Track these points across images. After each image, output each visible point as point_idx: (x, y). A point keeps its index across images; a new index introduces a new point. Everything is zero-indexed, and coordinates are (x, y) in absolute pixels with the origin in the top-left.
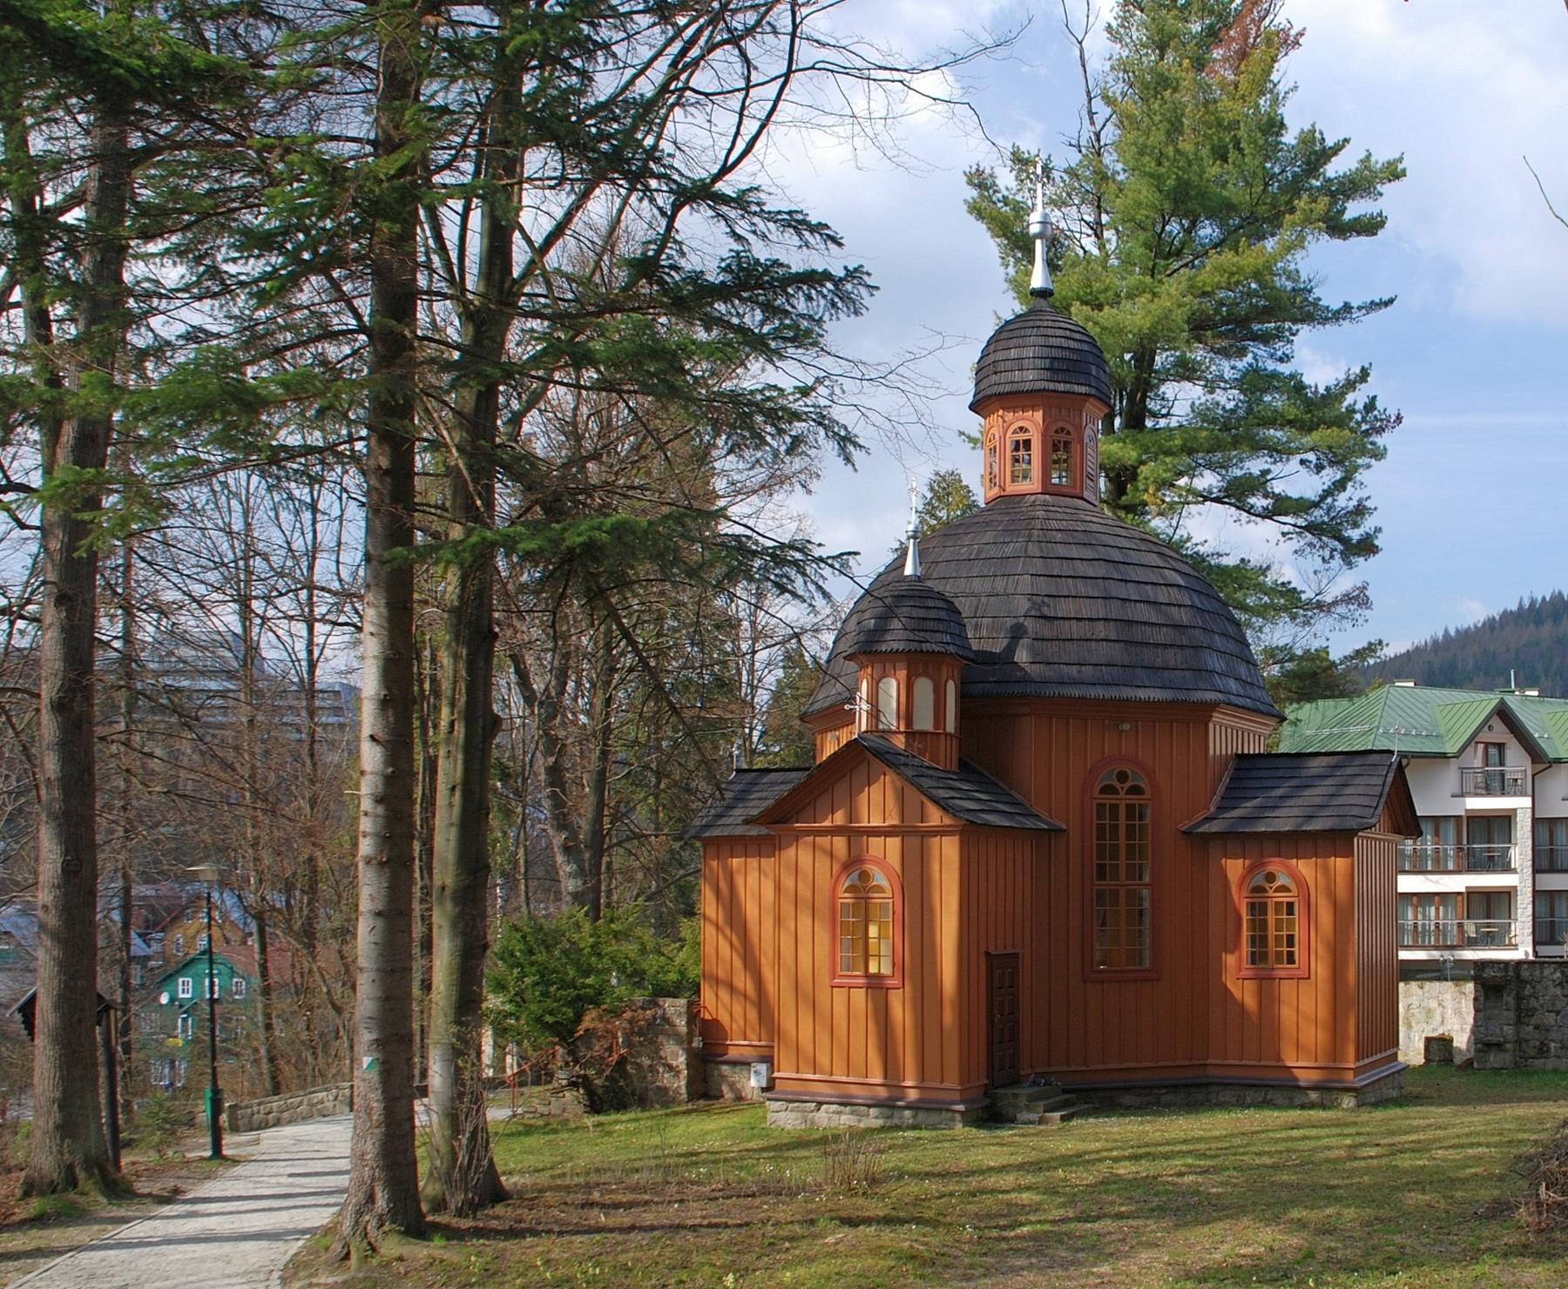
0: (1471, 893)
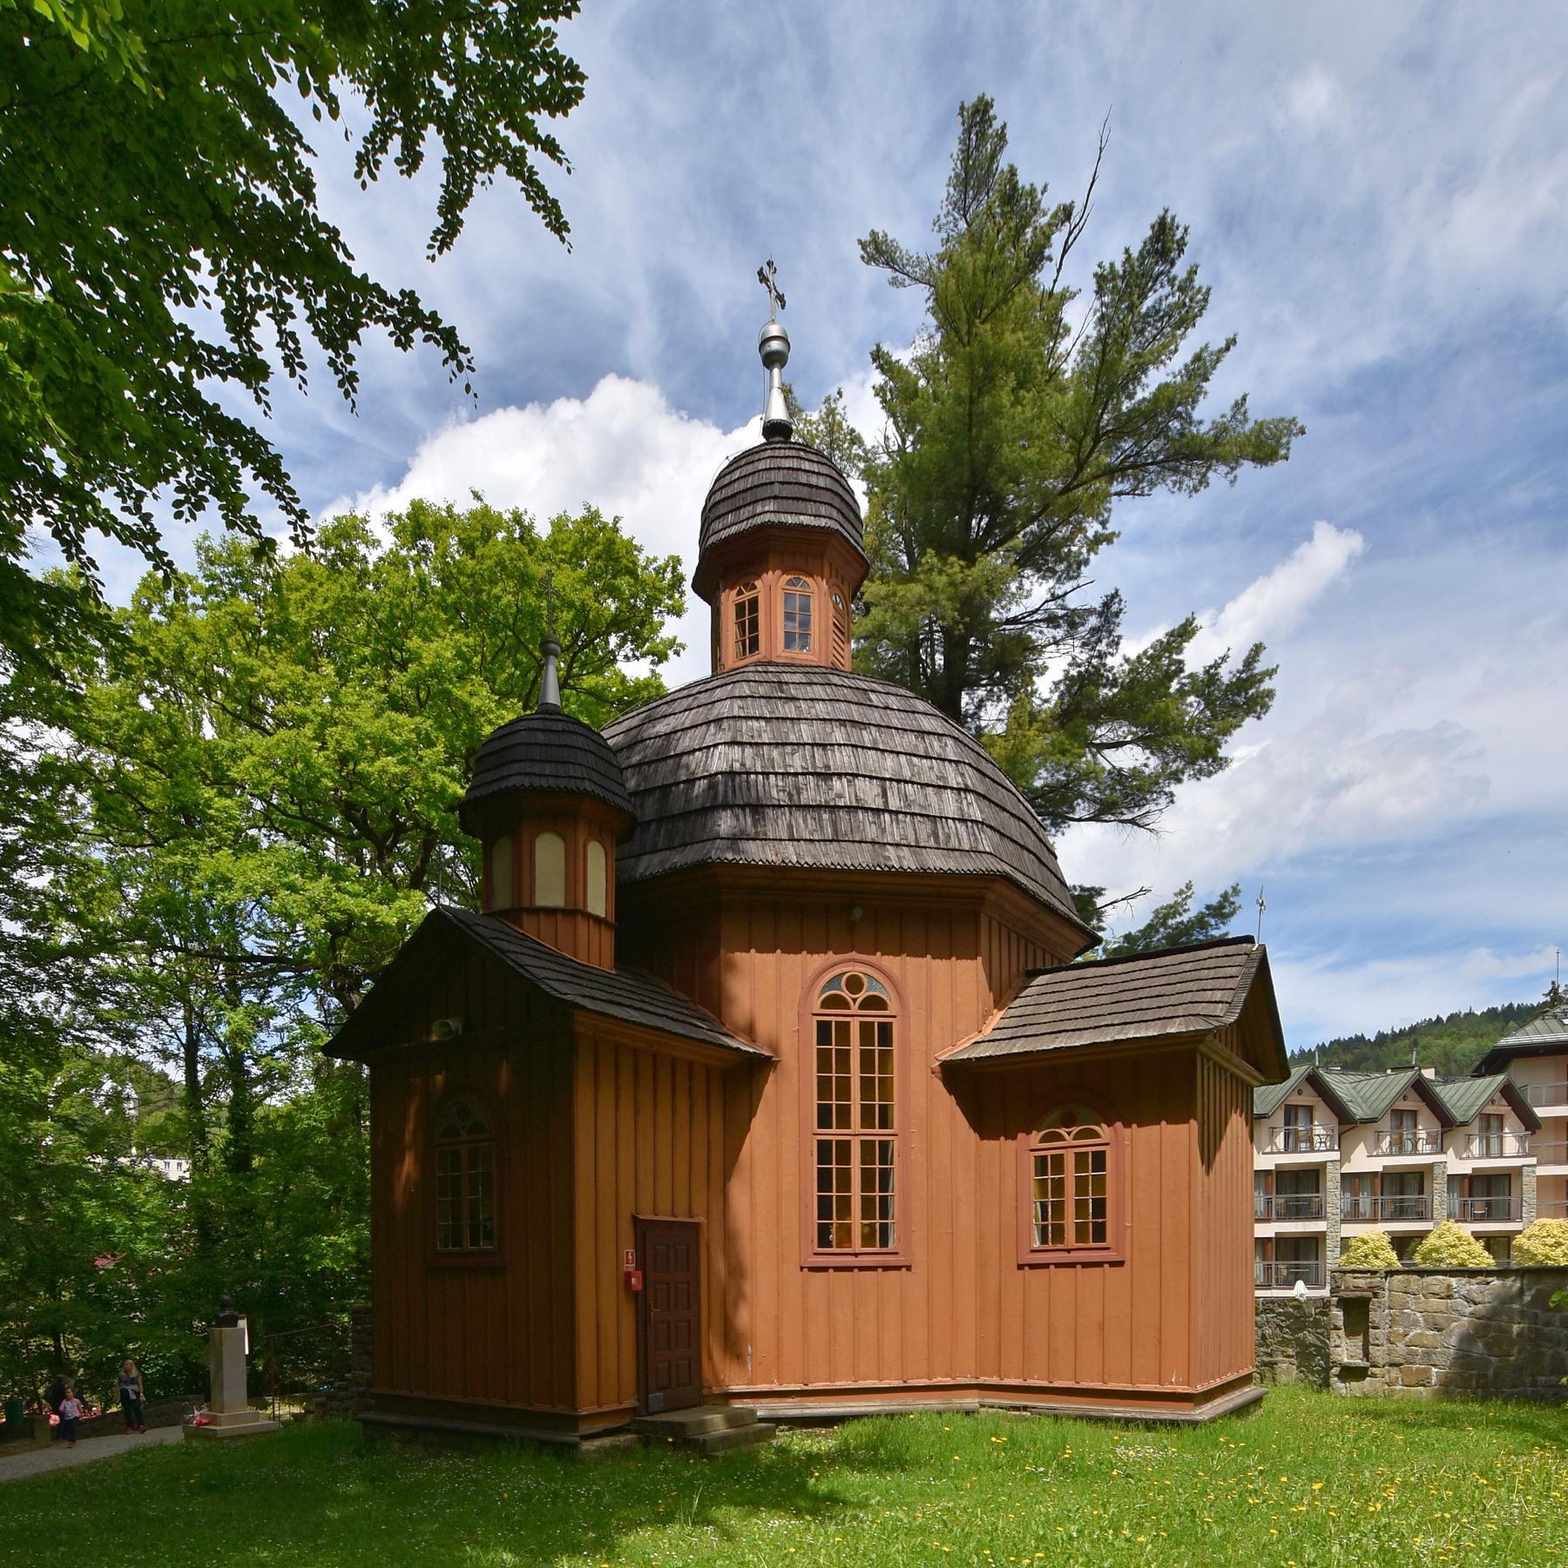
0: (1280, 1239)
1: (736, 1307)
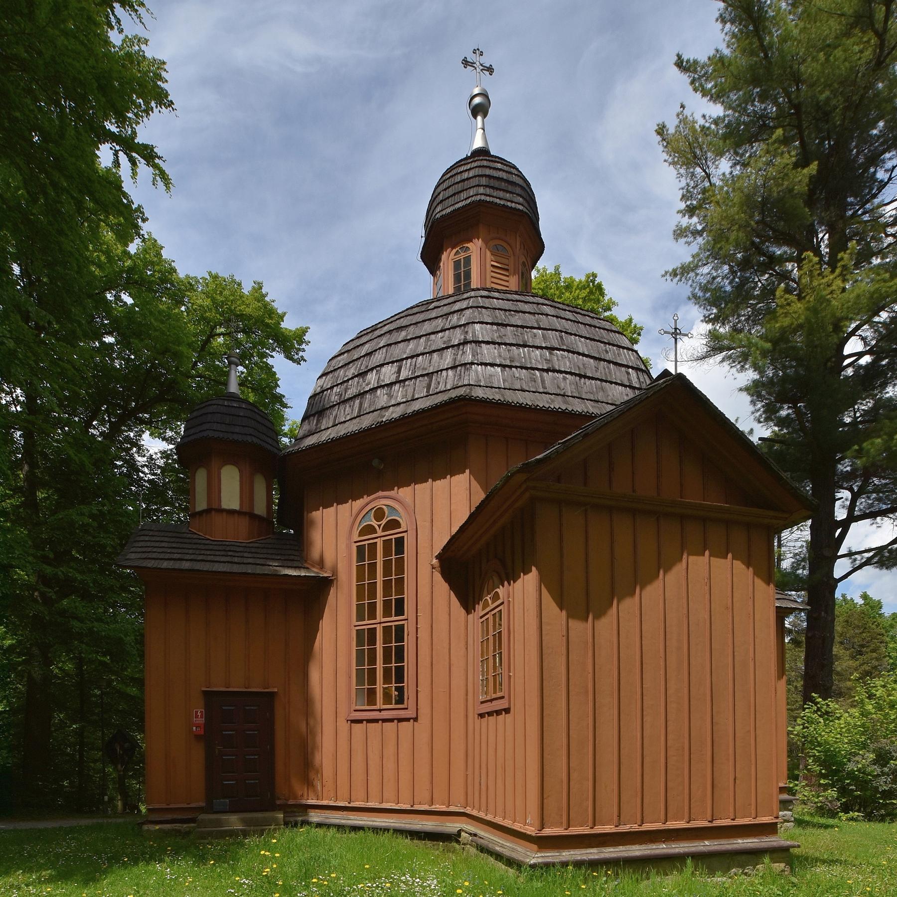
1: (313, 753)
